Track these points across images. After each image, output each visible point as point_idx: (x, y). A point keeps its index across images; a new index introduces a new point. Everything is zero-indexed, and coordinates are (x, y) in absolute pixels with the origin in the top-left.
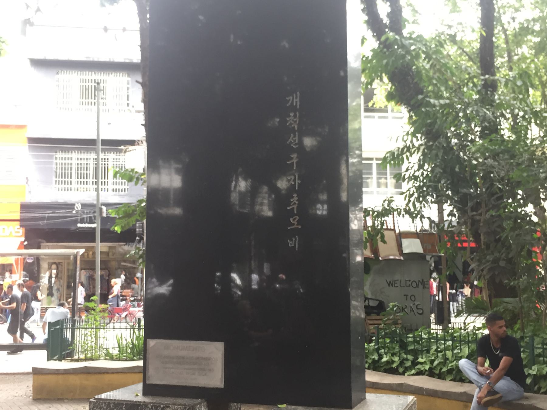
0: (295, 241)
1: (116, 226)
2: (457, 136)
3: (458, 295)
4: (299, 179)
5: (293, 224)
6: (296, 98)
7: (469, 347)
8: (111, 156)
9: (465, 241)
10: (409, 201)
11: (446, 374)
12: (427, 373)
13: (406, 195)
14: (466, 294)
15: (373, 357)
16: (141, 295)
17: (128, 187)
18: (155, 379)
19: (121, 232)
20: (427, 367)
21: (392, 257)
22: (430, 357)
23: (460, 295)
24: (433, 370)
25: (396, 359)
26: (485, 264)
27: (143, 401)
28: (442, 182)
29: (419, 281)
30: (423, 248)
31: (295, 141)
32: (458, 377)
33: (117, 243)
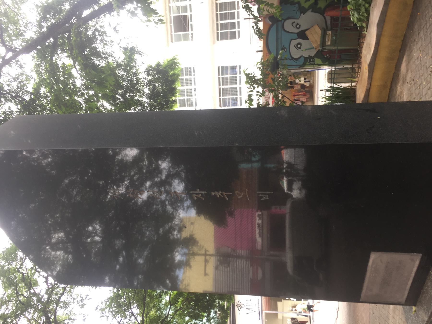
0: (262, 194)
4: (196, 191)
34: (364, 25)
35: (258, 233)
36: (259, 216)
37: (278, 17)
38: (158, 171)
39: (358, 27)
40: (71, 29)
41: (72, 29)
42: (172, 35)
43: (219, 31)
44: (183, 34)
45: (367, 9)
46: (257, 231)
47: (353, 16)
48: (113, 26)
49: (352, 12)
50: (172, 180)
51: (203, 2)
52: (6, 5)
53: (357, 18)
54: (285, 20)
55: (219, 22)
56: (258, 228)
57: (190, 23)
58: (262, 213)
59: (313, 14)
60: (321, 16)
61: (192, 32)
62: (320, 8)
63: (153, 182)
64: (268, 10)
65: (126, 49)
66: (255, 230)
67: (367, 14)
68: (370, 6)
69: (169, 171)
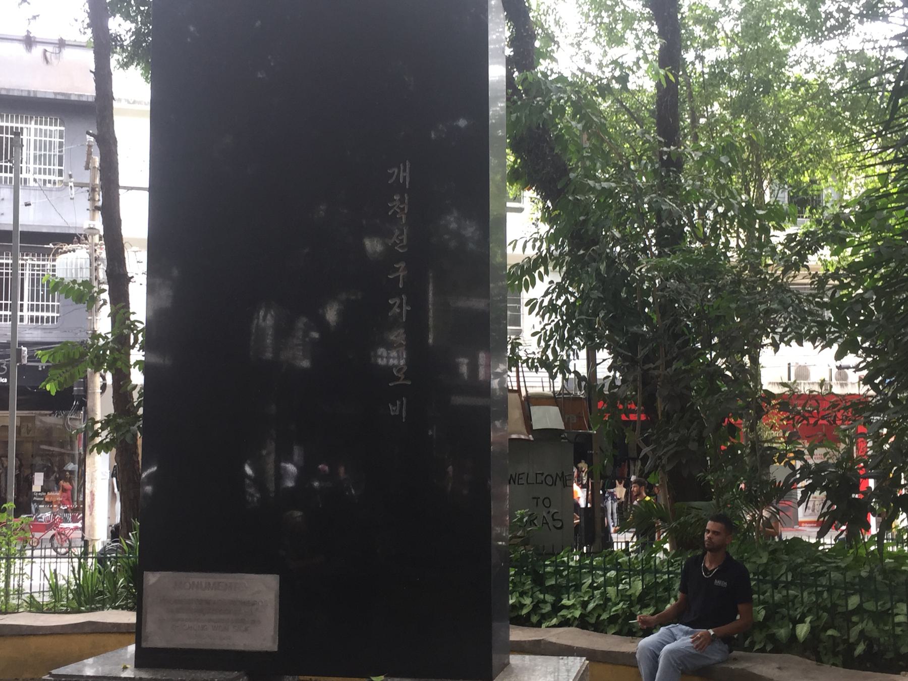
1: (47, 383)
2: (623, 242)
3: (607, 498)
4: (407, 304)
5: (398, 379)
6: (405, 171)
7: (643, 580)
8: (29, 261)
9: (633, 412)
10: (547, 346)
11: (606, 623)
12: (576, 623)
13: (541, 336)
14: (618, 497)
16: (77, 501)
17: (58, 315)
18: (156, 639)
19: (57, 392)
20: (577, 614)
21: (514, 436)
22: (581, 597)
23: (610, 498)
24: (587, 619)
25: (527, 601)
26: (665, 446)
27: (138, 677)
28: (601, 316)
29: (557, 474)
30: (564, 420)
31: (402, 241)
32: (626, 629)
33: (38, 412)
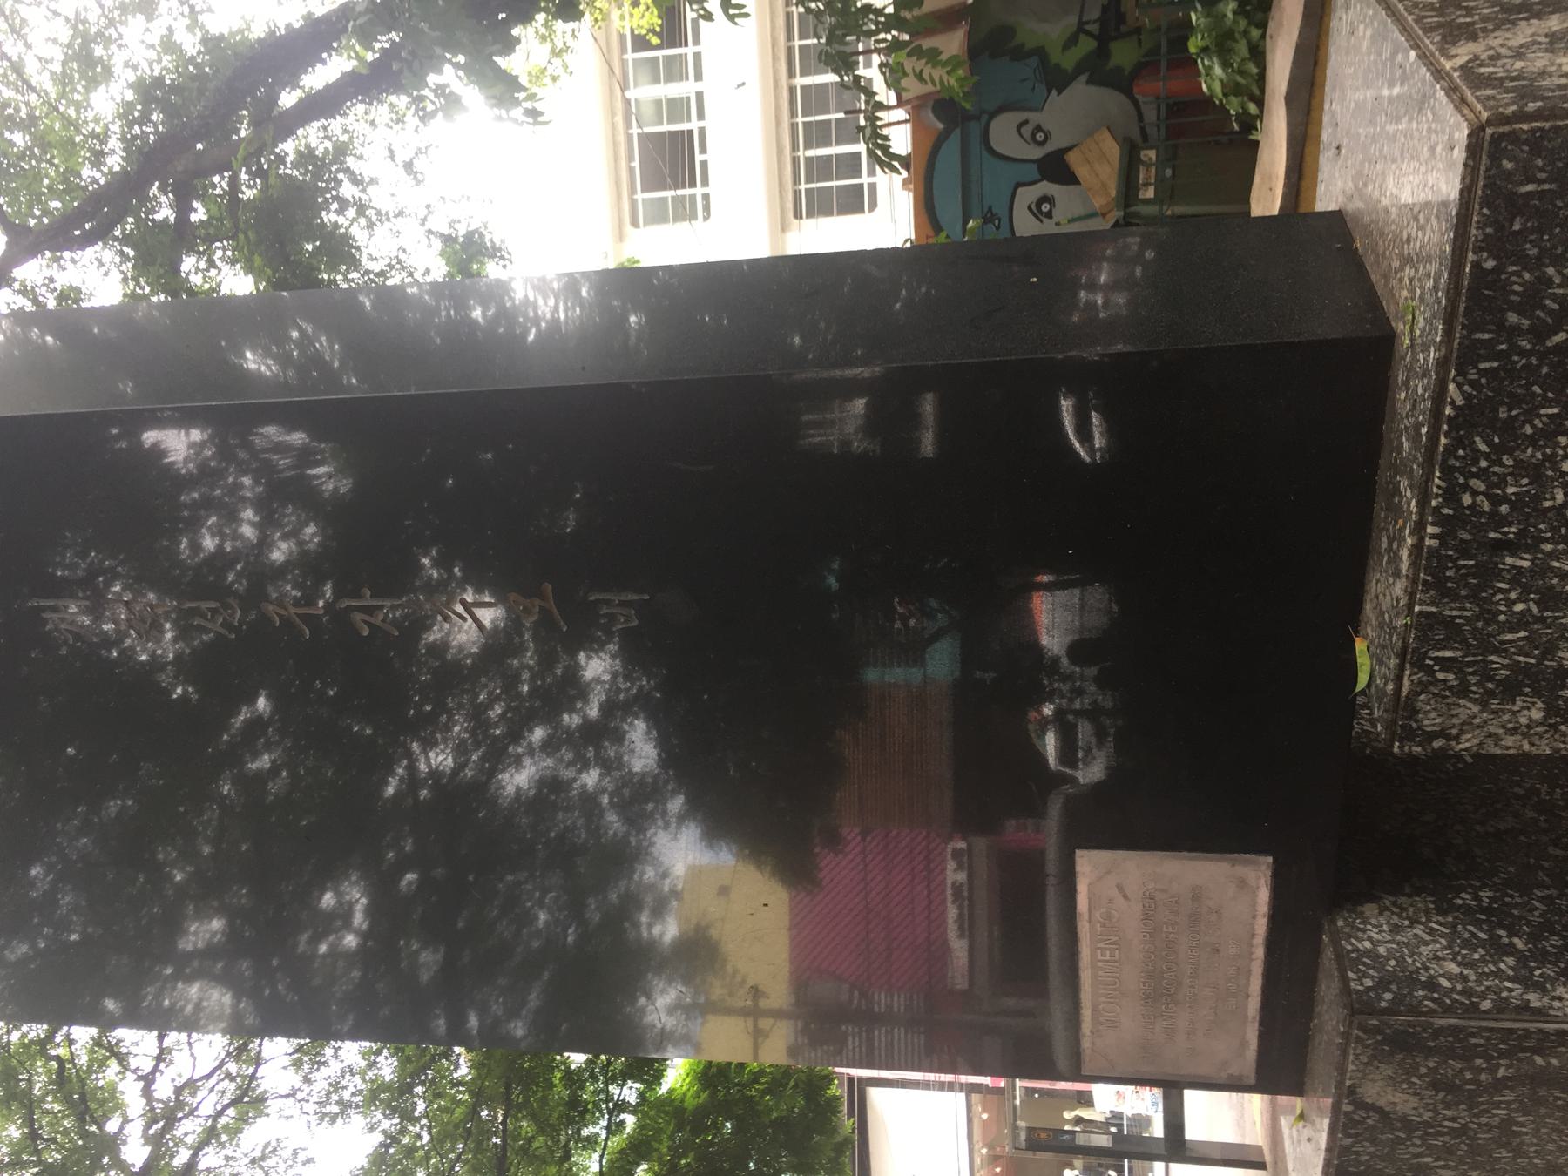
4: (360, 596)
15: (1230, 15)
31: (214, 611)
34: (1252, 108)
35: (955, 922)
36: (957, 854)
37: (956, 99)
38: (572, 689)
39: (1233, 118)
40: (233, 159)
41: (236, 159)
42: (633, 203)
43: (803, 187)
44: (673, 197)
45: (1258, 46)
46: (952, 912)
47: (1207, 75)
48: (402, 156)
49: (1202, 60)
50: (624, 720)
51: (744, 84)
52: (34, 90)
53: (1221, 81)
54: (992, 116)
55: (802, 154)
56: (954, 902)
57: (698, 158)
58: (969, 846)
59: (1095, 91)
60: (1115, 94)
61: (705, 190)
62: (1119, 70)
63: (555, 728)
64: (918, 71)
65: (448, 240)
66: (944, 912)
67: (1258, 67)
68: (1263, 36)
69: (613, 688)
